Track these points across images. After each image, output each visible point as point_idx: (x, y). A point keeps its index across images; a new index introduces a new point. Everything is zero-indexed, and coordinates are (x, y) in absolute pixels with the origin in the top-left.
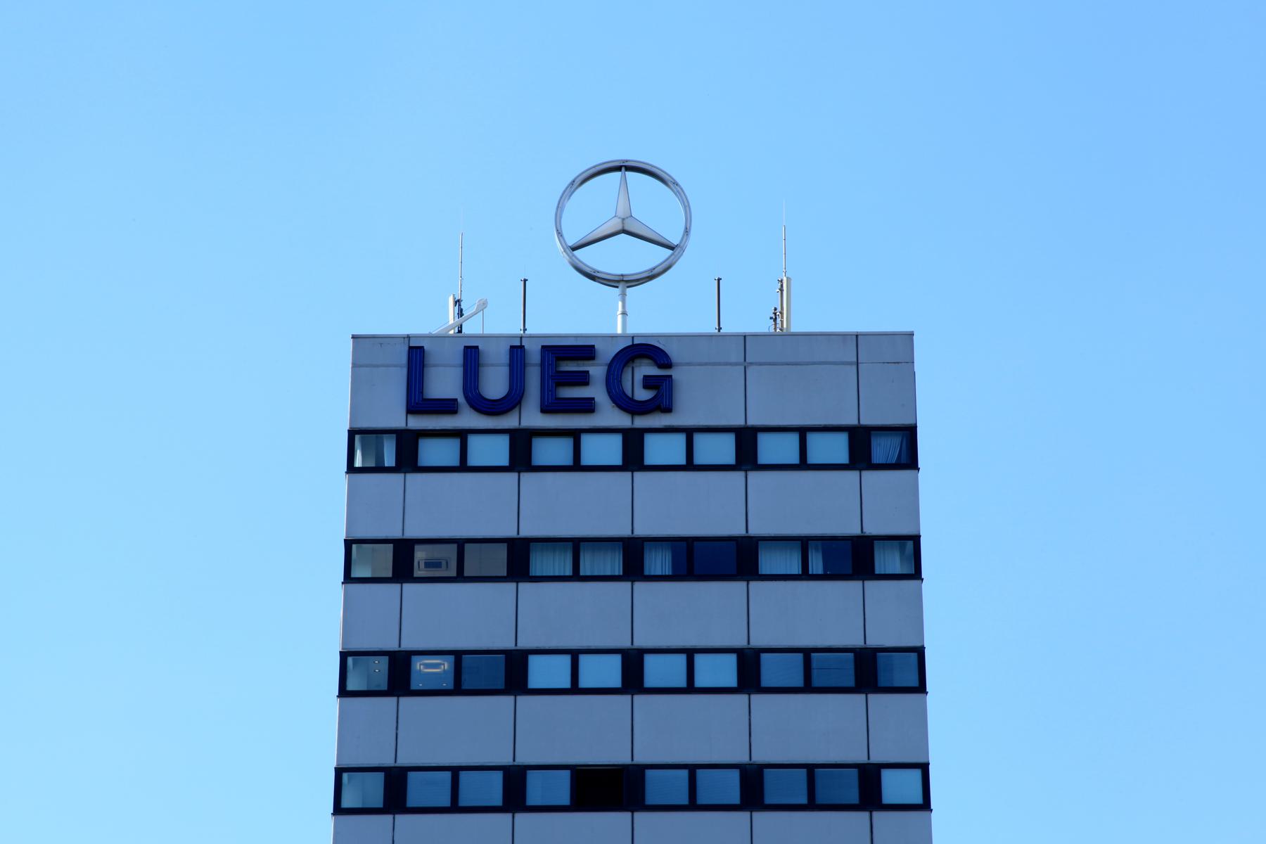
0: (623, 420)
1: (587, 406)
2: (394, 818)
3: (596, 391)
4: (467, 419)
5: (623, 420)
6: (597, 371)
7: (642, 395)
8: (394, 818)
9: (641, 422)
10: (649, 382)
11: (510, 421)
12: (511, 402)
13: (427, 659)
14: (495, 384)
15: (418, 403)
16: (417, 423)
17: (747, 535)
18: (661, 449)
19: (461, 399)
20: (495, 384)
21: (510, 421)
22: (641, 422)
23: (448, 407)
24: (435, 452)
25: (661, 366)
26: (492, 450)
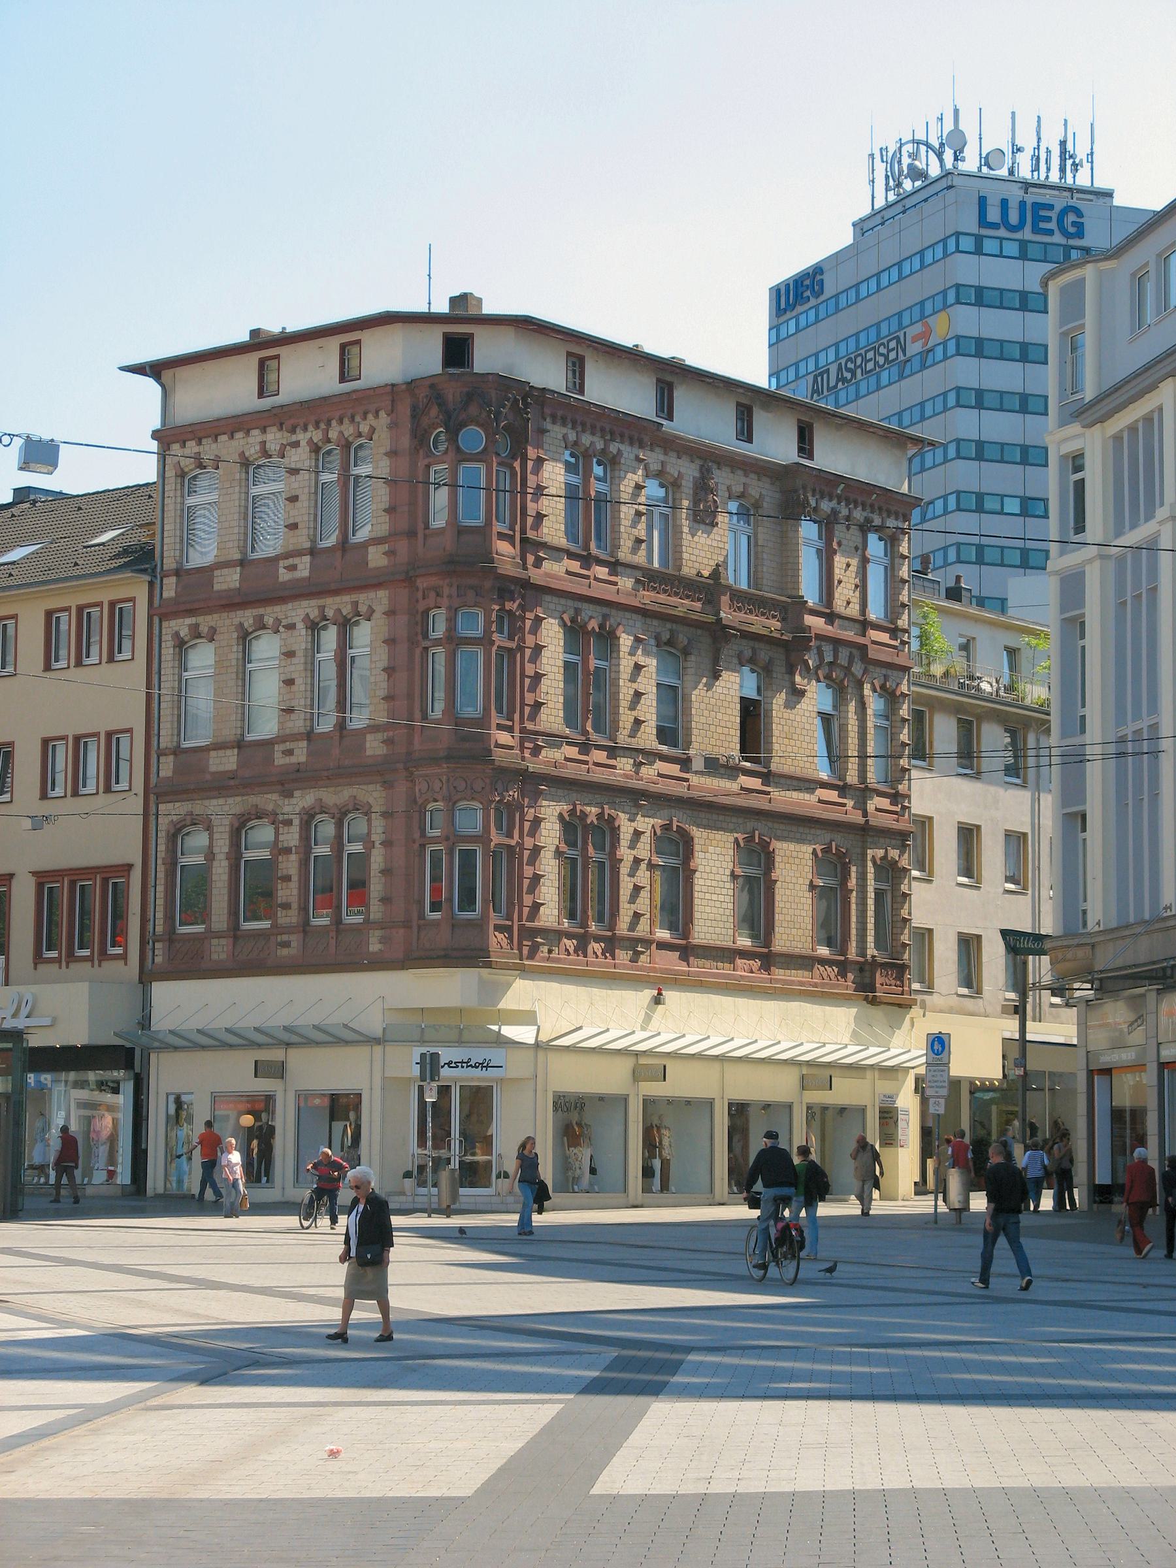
0: (1063, 241)
1: (1050, 232)
2: (341, 1286)
3: (1052, 225)
4: (1002, 232)
5: (1063, 241)
6: (1054, 215)
7: (1072, 230)
8: (341, 1286)
10: (1074, 224)
11: (1018, 236)
12: (1020, 226)
13: (686, 1340)
14: (1014, 218)
15: (983, 222)
16: (984, 232)
17: (283, 1200)
19: (802, 1179)
20: (1014, 218)
21: (1018, 236)
22: (1072, 242)
23: (994, 226)
24: (990, 246)
25: (1078, 217)
26: (1012, 248)
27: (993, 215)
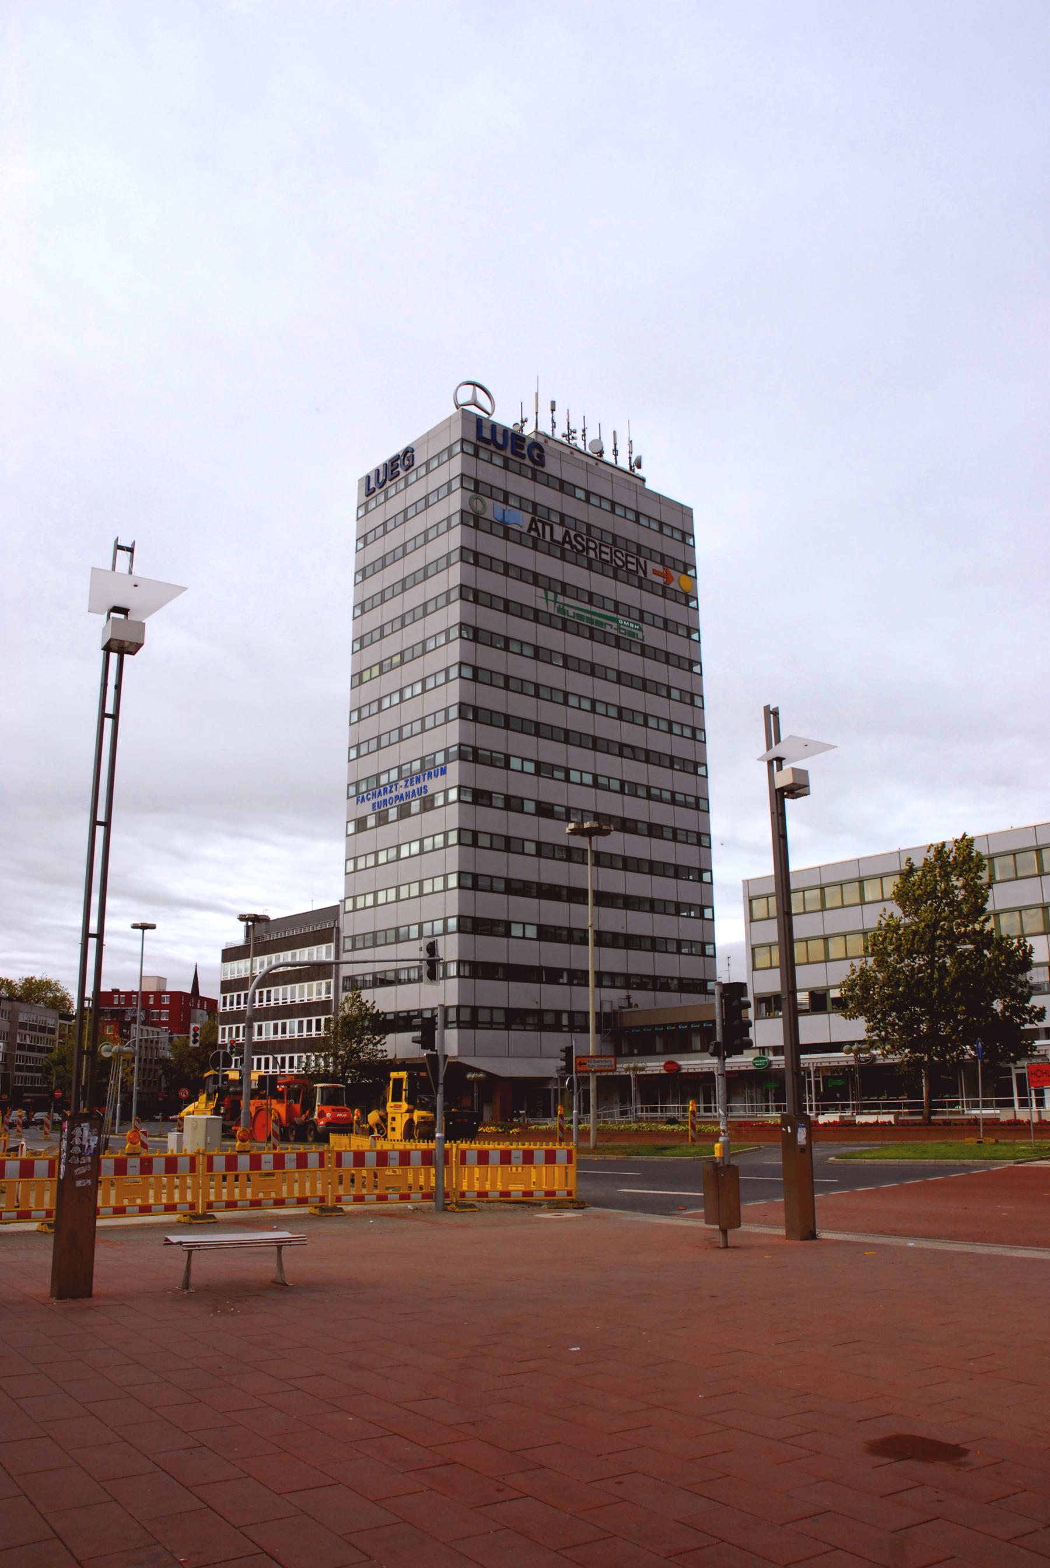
3: (525, 452)
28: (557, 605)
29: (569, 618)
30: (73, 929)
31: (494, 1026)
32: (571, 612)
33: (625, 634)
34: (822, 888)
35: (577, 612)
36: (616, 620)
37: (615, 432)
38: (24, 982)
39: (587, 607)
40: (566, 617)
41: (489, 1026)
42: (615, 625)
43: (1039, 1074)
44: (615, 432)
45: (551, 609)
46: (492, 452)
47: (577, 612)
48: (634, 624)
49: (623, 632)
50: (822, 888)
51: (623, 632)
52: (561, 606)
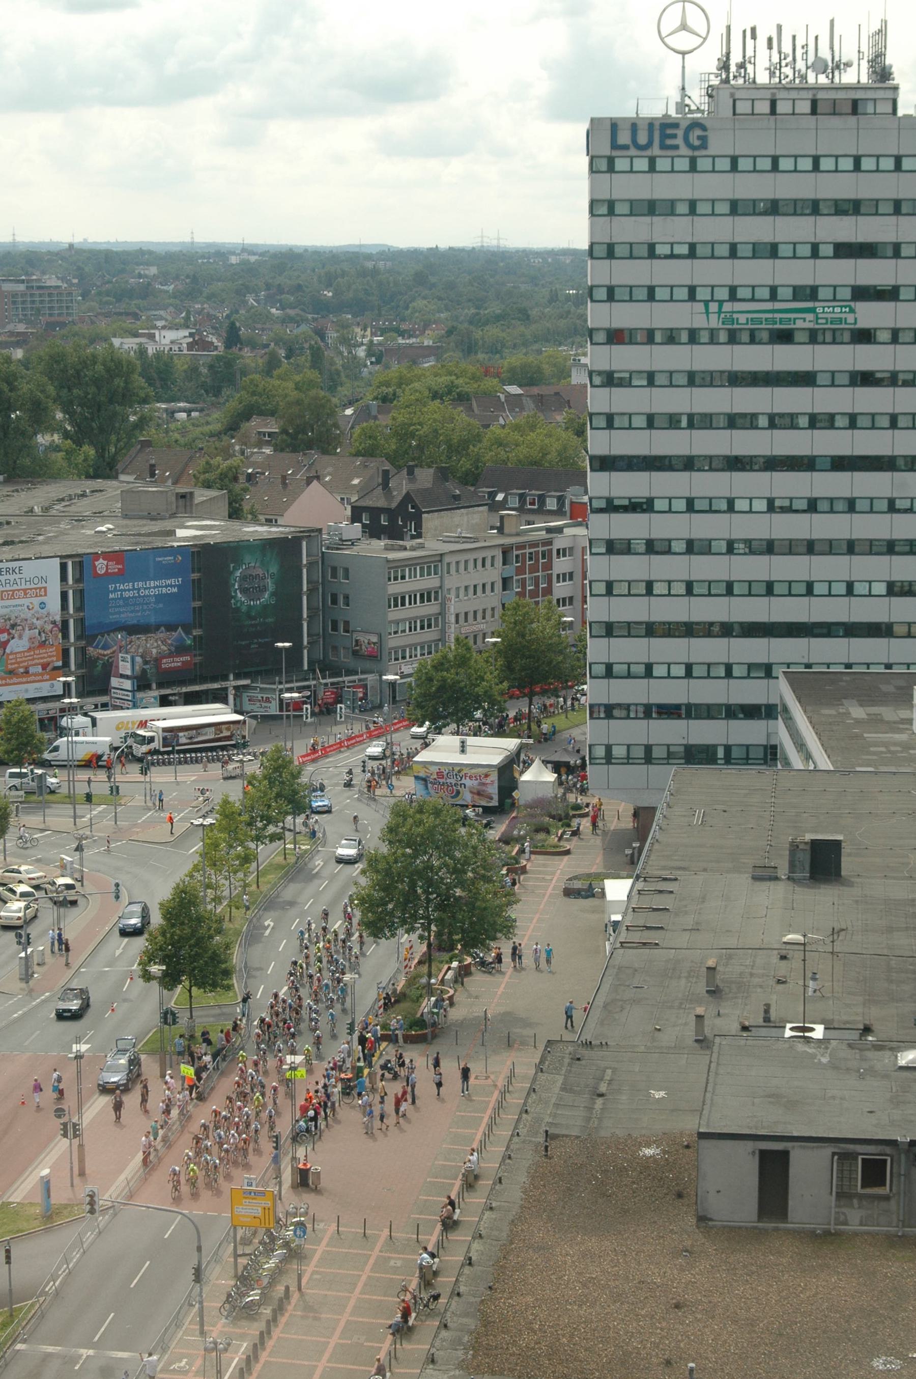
3: (679, 141)
4: (633, 152)
9: (697, 153)
11: (648, 153)
14: (642, 139)
18: (704, 164)
23: (625, 147)
27: (624, 138)
28: (723, 315)
29: (739, 326)
30: (850, 855)
31: (631, 761)
32: (742, 318)
33: (826, 323)
34: (751, 499)
35: (750, 316)
36: (812, 310)
37: (832, 22)
38: (500, 662)
39: (769, 306)
40: (735, 326)
41: (626, 761)
42: (810, 317)
43: (36, 581)
44: (832, 22)
45: (714, 322)
46: (632, 158)
47: (750, 316)
48: (841, 307)
49: (824, 321)
50: (751, 499)
51: (824, 321)
52: (728, 315)
